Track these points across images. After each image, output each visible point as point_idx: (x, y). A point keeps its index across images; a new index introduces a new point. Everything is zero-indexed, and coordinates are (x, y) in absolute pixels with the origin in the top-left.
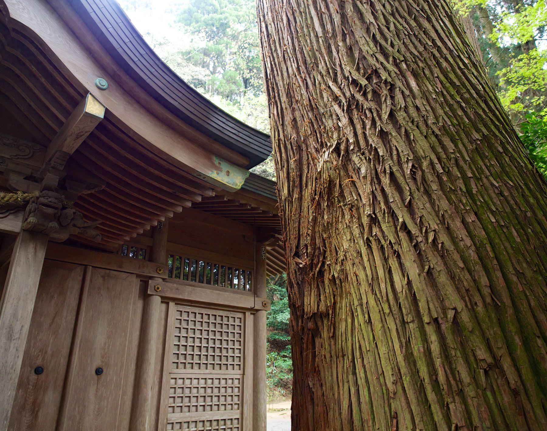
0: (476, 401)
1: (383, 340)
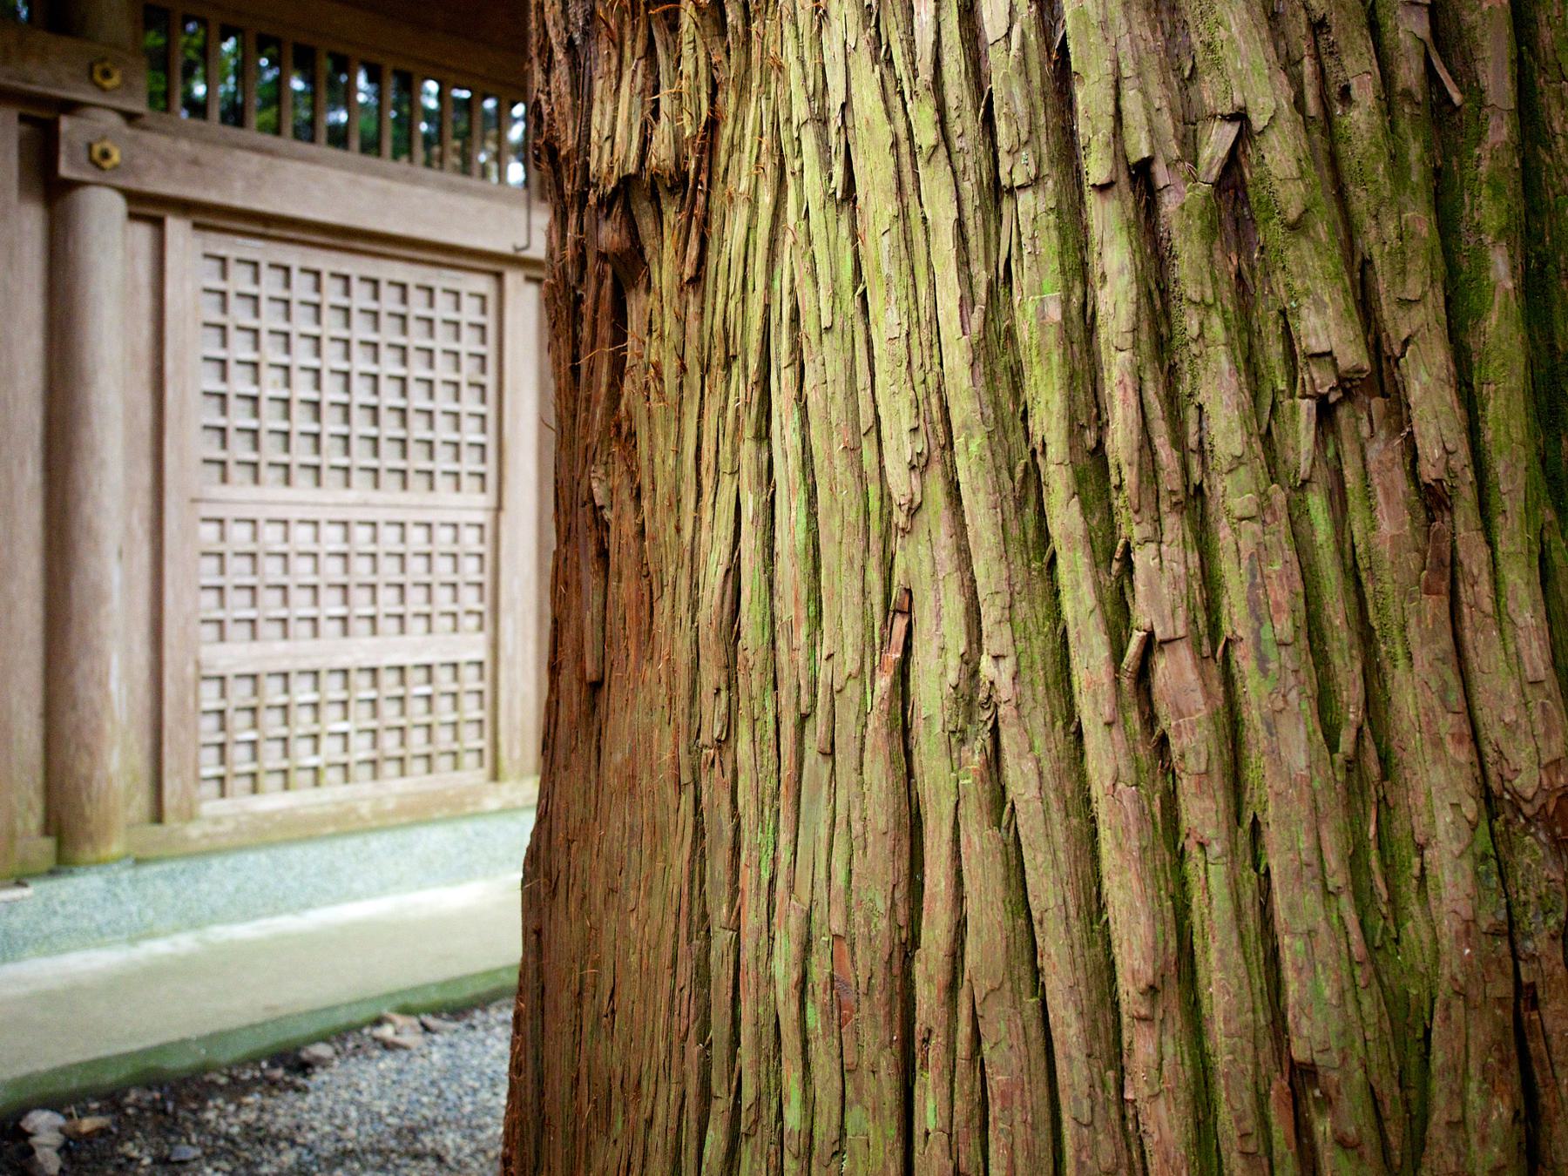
0: (1254, 534)
1: (895, 279)
